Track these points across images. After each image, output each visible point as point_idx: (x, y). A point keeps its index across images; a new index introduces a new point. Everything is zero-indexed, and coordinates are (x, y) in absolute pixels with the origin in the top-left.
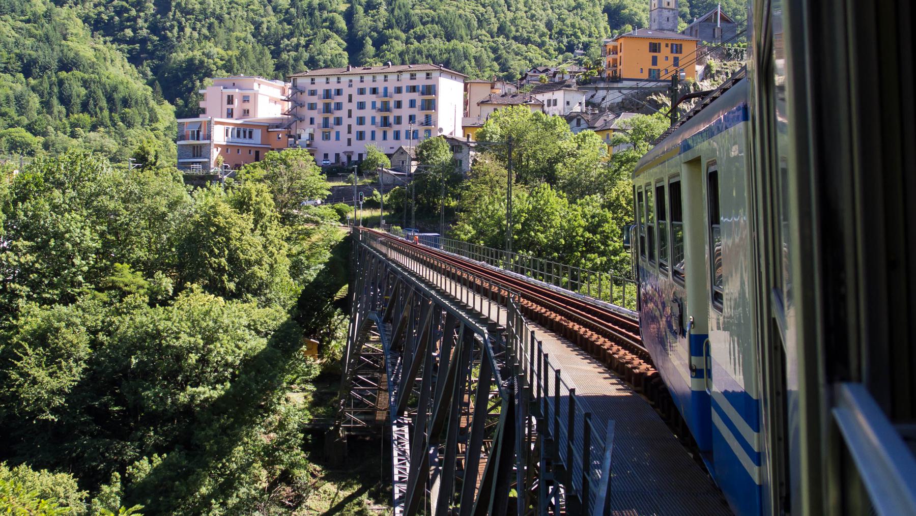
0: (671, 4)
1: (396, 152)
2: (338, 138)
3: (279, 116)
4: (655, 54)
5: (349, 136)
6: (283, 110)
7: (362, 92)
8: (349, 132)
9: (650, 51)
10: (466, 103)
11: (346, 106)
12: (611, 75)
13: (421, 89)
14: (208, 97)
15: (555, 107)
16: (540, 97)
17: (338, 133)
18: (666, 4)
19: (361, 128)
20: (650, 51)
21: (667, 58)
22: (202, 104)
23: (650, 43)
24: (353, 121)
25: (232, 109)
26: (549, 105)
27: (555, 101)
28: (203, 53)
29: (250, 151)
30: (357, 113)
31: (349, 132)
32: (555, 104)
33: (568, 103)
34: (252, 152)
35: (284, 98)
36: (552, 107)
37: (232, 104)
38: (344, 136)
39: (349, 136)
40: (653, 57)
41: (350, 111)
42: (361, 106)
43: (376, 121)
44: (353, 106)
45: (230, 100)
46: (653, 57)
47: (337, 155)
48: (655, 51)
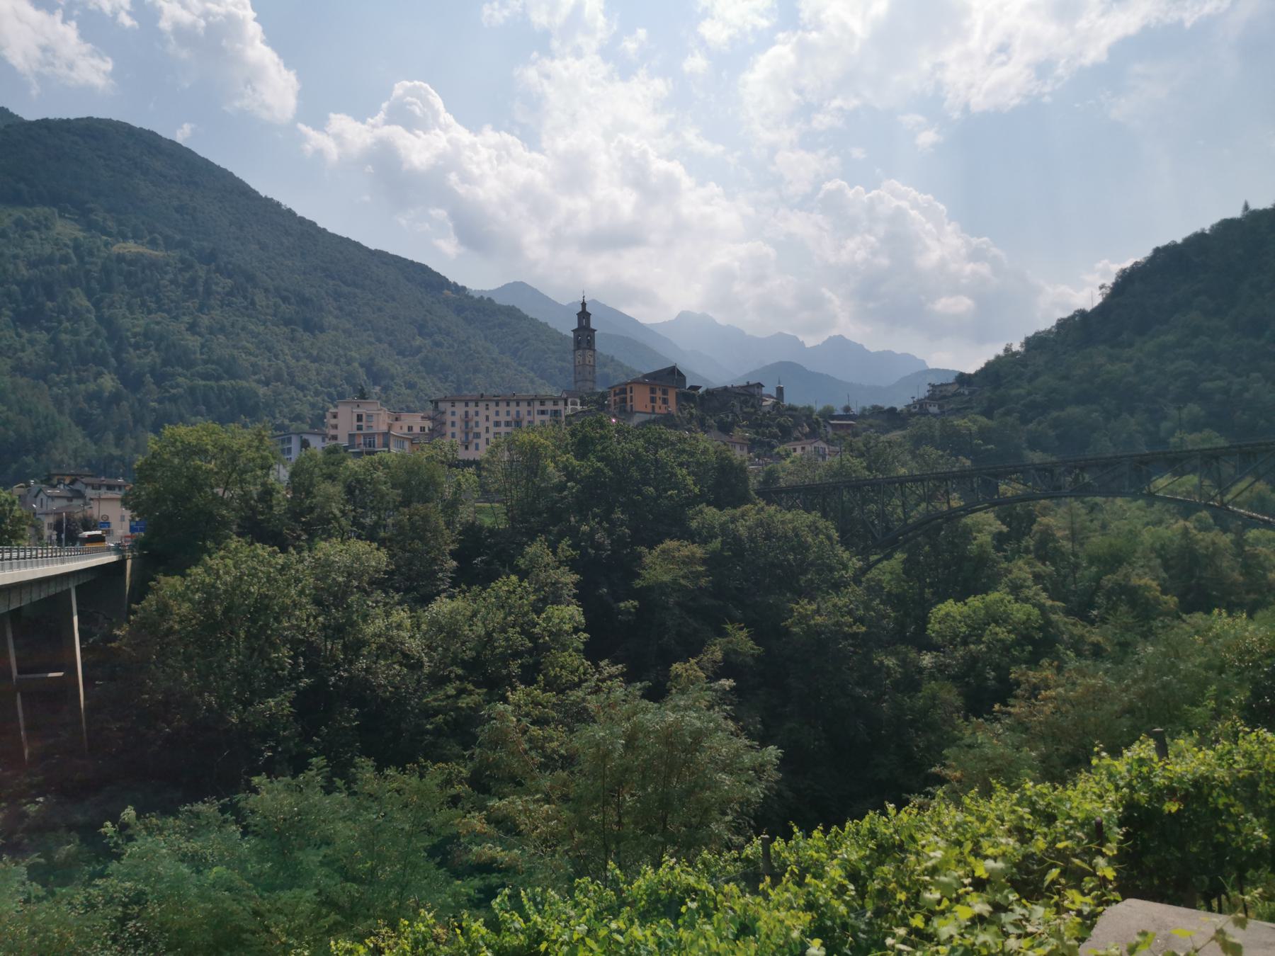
2: (477, 448)
7: (497, 424)
17: (477, 445)
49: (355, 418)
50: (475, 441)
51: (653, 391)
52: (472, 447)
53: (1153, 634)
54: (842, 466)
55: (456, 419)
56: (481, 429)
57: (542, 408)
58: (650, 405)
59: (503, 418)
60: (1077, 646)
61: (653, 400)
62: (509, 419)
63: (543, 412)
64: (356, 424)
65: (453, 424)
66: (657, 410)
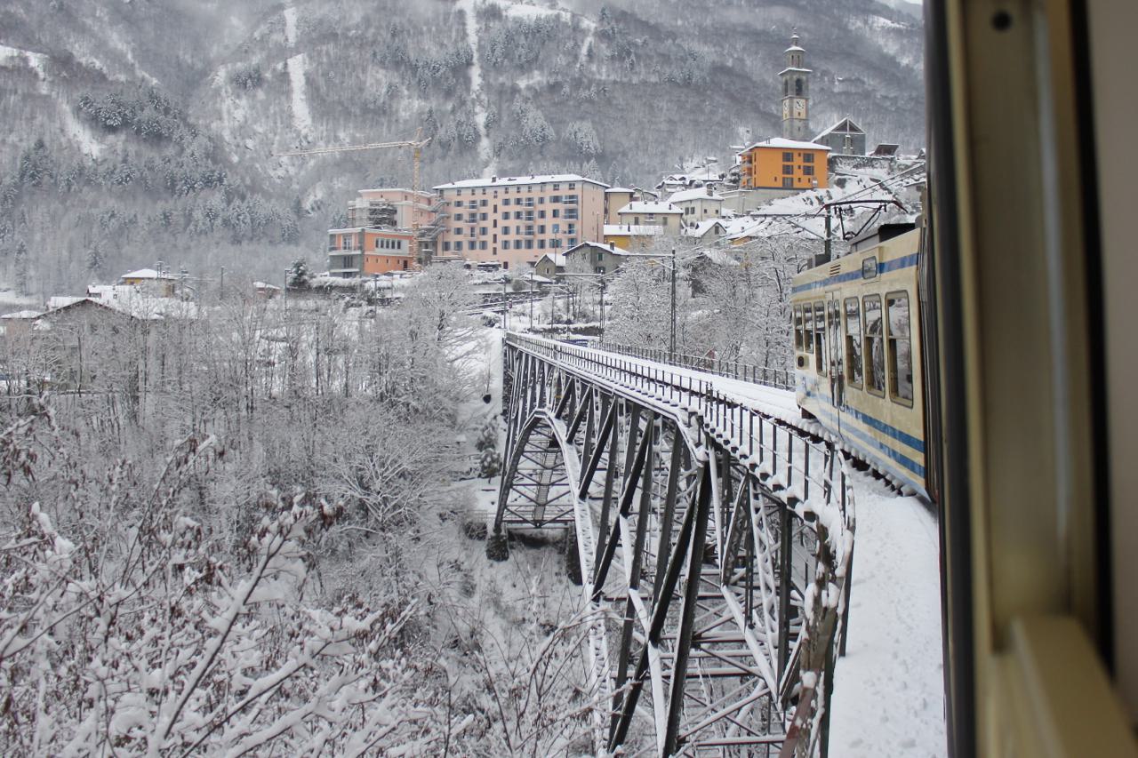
5: (495, 245)
8: (495, 241)
19: (506, 238)
21: (799, 167)
27: (693, 209)
31: (495, 241)
32: (693, 212)
33: (706, 211)
36: (690, 215)
44: (499, 216)
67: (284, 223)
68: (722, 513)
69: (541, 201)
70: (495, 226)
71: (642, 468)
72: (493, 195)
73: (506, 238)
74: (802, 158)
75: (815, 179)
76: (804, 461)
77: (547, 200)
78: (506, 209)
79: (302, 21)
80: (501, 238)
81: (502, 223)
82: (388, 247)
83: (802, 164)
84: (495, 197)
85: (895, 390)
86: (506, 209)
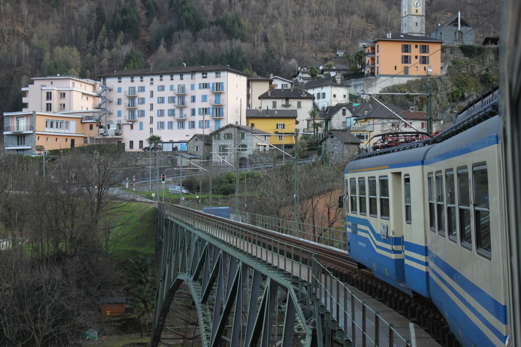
0: (419, 11)
1: (192, 139)
2: (141, 128)
3: (91, 109)
4: (406, 65)
5: (151, 126)
6: (94, 104)
7: (161, 100)
8: (151, 122)
9: (402, 63)
10: (248, 96)
11: (148, 101)
12: (370, 72)
13: (211, 86)
14: (30, 94)
15: (323, 100)
16: (311, 92)
17: (141, 124)
18: (415, 11)
19: (161, 119)
20: (402, 63)
21: (416, 57)
22: (24, 100)
23: (402, 45)
24: (154, 113)
25: (51, 104)
26: (319, 98)
27: (324, 94)
28: (24, 329)
29: (66, 139)
30: (157, 107)
31: (151, 122)
32: (324, 97)
33: (335, 96)
34: (68, 140)
35: (95, 94)
36: (321, 100)
37: (51, 99)
38: (147, 126)
39: (151, 126)
40: (405, 67)
41: (152, 105)
42: (161, 113)
43: (174, 88)
44: (154, 101)
45: (49, 96)
46: (405, 67)
47: (141, 142)
48: (406, 51)
49: (45, 95)
50: (140, 119)
51: (406, 49)
52: (136, 126)
53: (194, 35)
54: (371, 7)
55: (122, 96)
56: (145, 107)
57: (205, 81)
58: (401, 67)
59: (167, 94)
60: (7, 329)
61: (406, 60)
62: (206, 105)
63: (205, 86)
64: (45, 102)
65: (119, 102)
66: (412, 71)
67: (164, 217)
68: (486, 203)
69: (193, 87)
70: (152, 109)
71: (164, 291)
72: (149, 82)
73: (161, 119)
74: (418, 49)
75: (430, 67)
76: (361, 320)
77: (197, 87)
78: (161, 94)
79: (235, 194)
80: (156, 120)
81: (157, 107)
82: (52, 127)
83: (420, 55)
84: (152, 84)
85: (479, 244)
86: (161, 94)
